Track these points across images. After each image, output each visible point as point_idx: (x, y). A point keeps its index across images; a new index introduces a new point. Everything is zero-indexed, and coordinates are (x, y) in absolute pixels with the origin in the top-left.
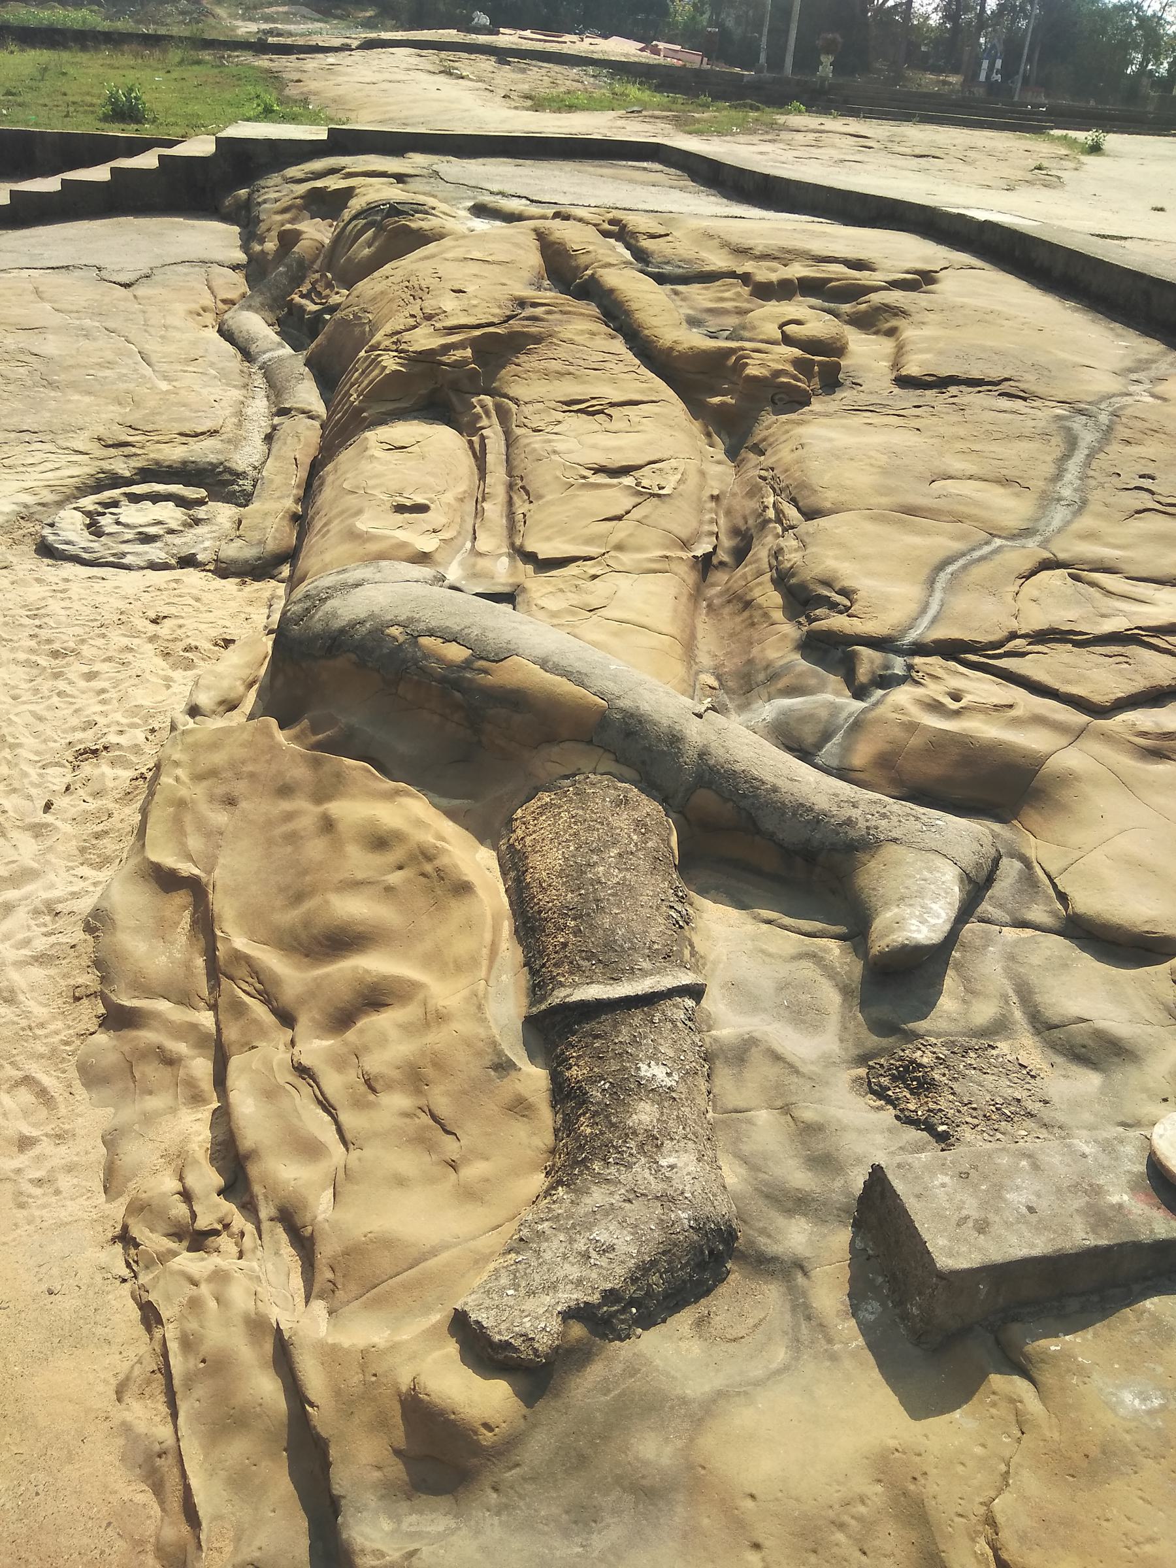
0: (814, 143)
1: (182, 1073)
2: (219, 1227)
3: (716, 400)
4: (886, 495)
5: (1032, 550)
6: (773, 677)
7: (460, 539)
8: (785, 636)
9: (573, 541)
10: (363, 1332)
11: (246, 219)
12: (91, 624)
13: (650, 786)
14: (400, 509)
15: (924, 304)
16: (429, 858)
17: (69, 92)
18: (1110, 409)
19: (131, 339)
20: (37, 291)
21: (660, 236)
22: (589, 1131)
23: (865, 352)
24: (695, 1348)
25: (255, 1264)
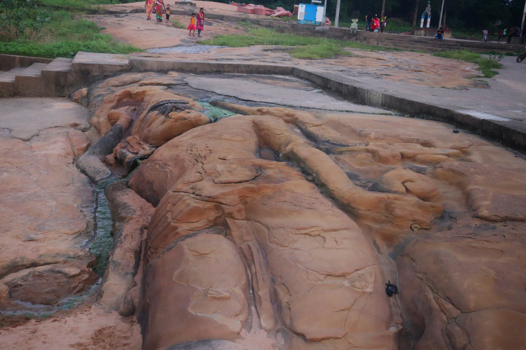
11: (86, 102)
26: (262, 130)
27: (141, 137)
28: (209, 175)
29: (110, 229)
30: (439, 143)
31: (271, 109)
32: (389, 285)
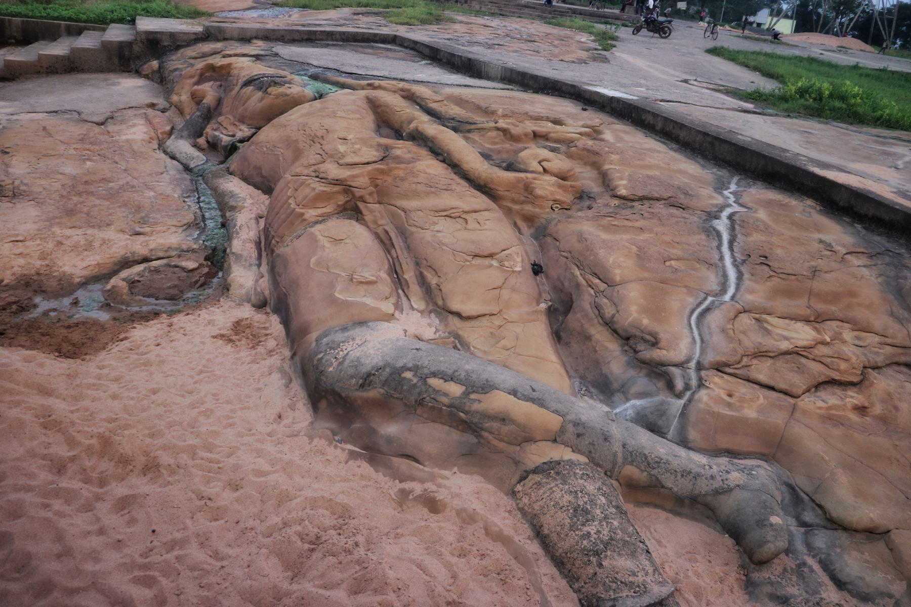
26: (379, 106)
27: (235, 117)
28: (331, 156)
29: (220, 220)
30: (570, 121)
31: (383, 83)
32: (534, 265)
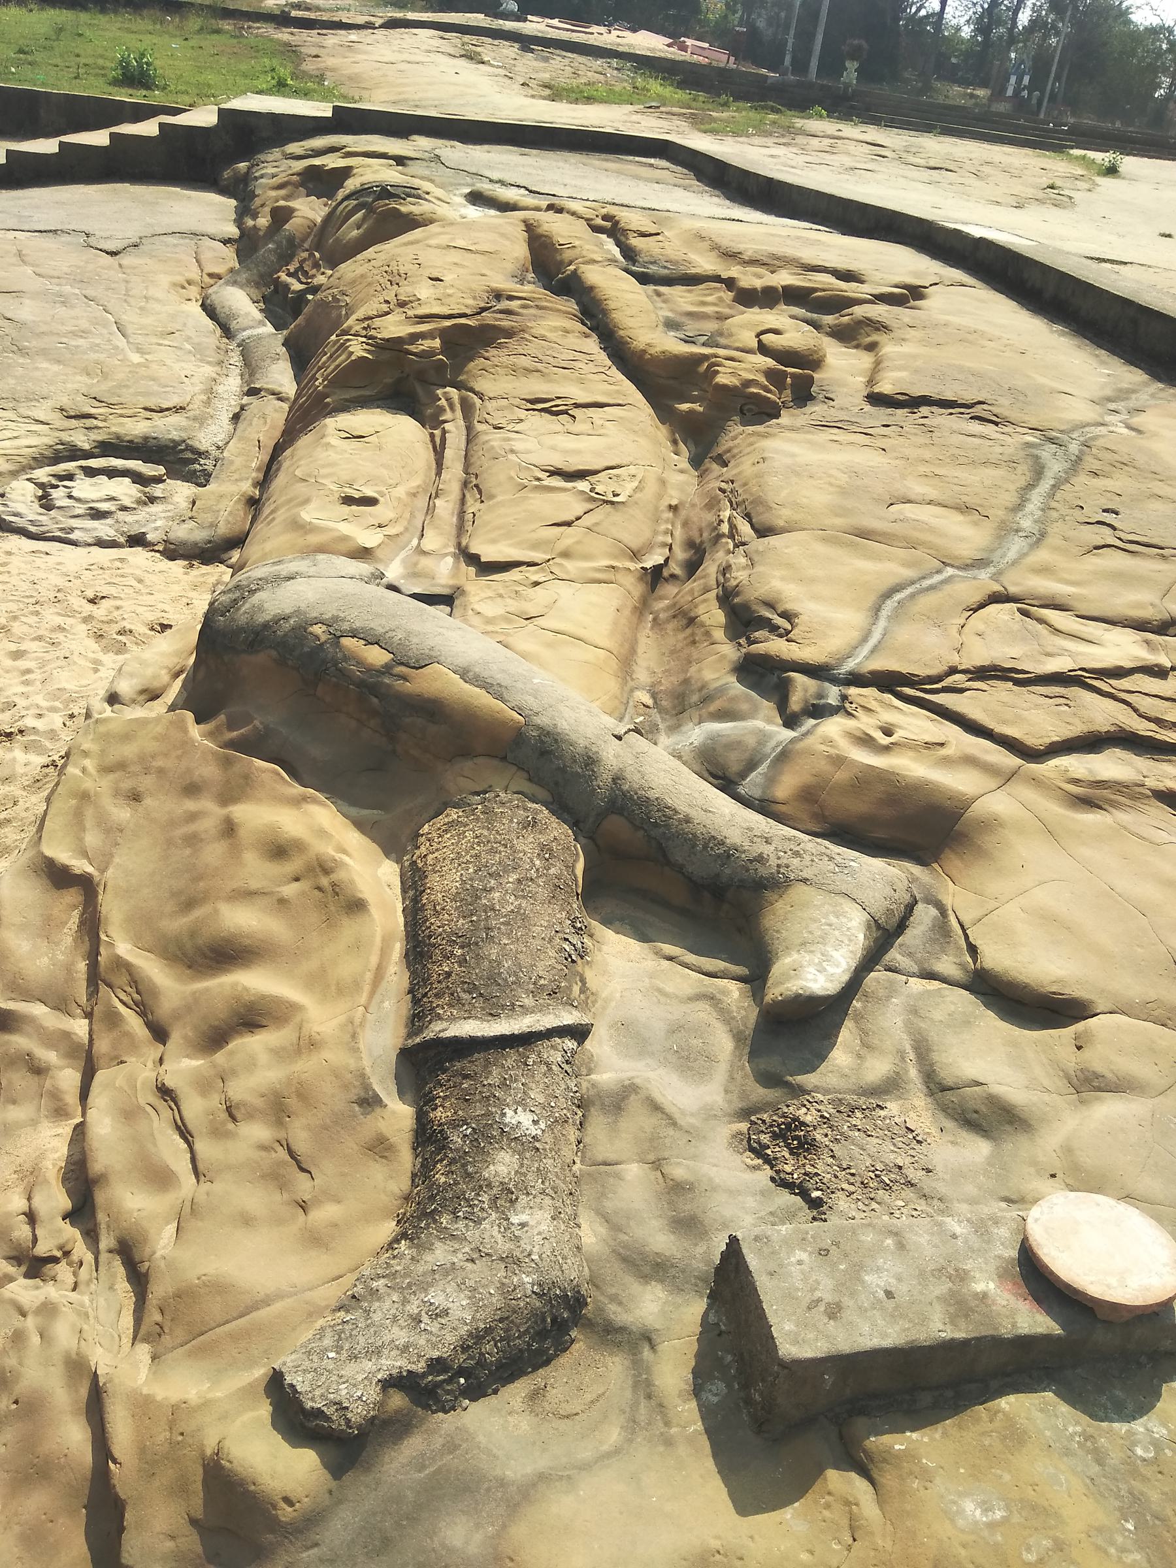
0: (828, 149)
1: (48, 1084)
2: (59, 1254)
3: (685, 407)
4: (837, 515)
5: (984, 581)
6: (706, 700)
7: (407, 535)
8: (724, 657)
9: (519, 545)
10: (184, 1384)
11: (241, 191)
12: (26, 600)
13: (561, 808)
14: (348, 500)
15: (907, 320)
16: (327, 871)
17: (82, 52)
18: (1082, 439)
19: (110, 308)
20: (20, 254)
21: (651, 235)
22: (443, 1179)
23: (843, 367)
24: (524, 1424)
25: (86, 1299)
